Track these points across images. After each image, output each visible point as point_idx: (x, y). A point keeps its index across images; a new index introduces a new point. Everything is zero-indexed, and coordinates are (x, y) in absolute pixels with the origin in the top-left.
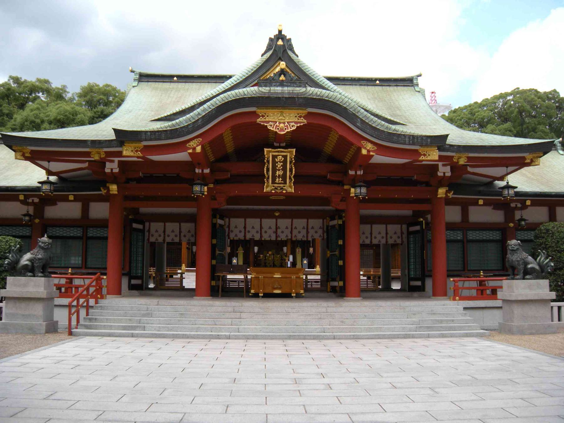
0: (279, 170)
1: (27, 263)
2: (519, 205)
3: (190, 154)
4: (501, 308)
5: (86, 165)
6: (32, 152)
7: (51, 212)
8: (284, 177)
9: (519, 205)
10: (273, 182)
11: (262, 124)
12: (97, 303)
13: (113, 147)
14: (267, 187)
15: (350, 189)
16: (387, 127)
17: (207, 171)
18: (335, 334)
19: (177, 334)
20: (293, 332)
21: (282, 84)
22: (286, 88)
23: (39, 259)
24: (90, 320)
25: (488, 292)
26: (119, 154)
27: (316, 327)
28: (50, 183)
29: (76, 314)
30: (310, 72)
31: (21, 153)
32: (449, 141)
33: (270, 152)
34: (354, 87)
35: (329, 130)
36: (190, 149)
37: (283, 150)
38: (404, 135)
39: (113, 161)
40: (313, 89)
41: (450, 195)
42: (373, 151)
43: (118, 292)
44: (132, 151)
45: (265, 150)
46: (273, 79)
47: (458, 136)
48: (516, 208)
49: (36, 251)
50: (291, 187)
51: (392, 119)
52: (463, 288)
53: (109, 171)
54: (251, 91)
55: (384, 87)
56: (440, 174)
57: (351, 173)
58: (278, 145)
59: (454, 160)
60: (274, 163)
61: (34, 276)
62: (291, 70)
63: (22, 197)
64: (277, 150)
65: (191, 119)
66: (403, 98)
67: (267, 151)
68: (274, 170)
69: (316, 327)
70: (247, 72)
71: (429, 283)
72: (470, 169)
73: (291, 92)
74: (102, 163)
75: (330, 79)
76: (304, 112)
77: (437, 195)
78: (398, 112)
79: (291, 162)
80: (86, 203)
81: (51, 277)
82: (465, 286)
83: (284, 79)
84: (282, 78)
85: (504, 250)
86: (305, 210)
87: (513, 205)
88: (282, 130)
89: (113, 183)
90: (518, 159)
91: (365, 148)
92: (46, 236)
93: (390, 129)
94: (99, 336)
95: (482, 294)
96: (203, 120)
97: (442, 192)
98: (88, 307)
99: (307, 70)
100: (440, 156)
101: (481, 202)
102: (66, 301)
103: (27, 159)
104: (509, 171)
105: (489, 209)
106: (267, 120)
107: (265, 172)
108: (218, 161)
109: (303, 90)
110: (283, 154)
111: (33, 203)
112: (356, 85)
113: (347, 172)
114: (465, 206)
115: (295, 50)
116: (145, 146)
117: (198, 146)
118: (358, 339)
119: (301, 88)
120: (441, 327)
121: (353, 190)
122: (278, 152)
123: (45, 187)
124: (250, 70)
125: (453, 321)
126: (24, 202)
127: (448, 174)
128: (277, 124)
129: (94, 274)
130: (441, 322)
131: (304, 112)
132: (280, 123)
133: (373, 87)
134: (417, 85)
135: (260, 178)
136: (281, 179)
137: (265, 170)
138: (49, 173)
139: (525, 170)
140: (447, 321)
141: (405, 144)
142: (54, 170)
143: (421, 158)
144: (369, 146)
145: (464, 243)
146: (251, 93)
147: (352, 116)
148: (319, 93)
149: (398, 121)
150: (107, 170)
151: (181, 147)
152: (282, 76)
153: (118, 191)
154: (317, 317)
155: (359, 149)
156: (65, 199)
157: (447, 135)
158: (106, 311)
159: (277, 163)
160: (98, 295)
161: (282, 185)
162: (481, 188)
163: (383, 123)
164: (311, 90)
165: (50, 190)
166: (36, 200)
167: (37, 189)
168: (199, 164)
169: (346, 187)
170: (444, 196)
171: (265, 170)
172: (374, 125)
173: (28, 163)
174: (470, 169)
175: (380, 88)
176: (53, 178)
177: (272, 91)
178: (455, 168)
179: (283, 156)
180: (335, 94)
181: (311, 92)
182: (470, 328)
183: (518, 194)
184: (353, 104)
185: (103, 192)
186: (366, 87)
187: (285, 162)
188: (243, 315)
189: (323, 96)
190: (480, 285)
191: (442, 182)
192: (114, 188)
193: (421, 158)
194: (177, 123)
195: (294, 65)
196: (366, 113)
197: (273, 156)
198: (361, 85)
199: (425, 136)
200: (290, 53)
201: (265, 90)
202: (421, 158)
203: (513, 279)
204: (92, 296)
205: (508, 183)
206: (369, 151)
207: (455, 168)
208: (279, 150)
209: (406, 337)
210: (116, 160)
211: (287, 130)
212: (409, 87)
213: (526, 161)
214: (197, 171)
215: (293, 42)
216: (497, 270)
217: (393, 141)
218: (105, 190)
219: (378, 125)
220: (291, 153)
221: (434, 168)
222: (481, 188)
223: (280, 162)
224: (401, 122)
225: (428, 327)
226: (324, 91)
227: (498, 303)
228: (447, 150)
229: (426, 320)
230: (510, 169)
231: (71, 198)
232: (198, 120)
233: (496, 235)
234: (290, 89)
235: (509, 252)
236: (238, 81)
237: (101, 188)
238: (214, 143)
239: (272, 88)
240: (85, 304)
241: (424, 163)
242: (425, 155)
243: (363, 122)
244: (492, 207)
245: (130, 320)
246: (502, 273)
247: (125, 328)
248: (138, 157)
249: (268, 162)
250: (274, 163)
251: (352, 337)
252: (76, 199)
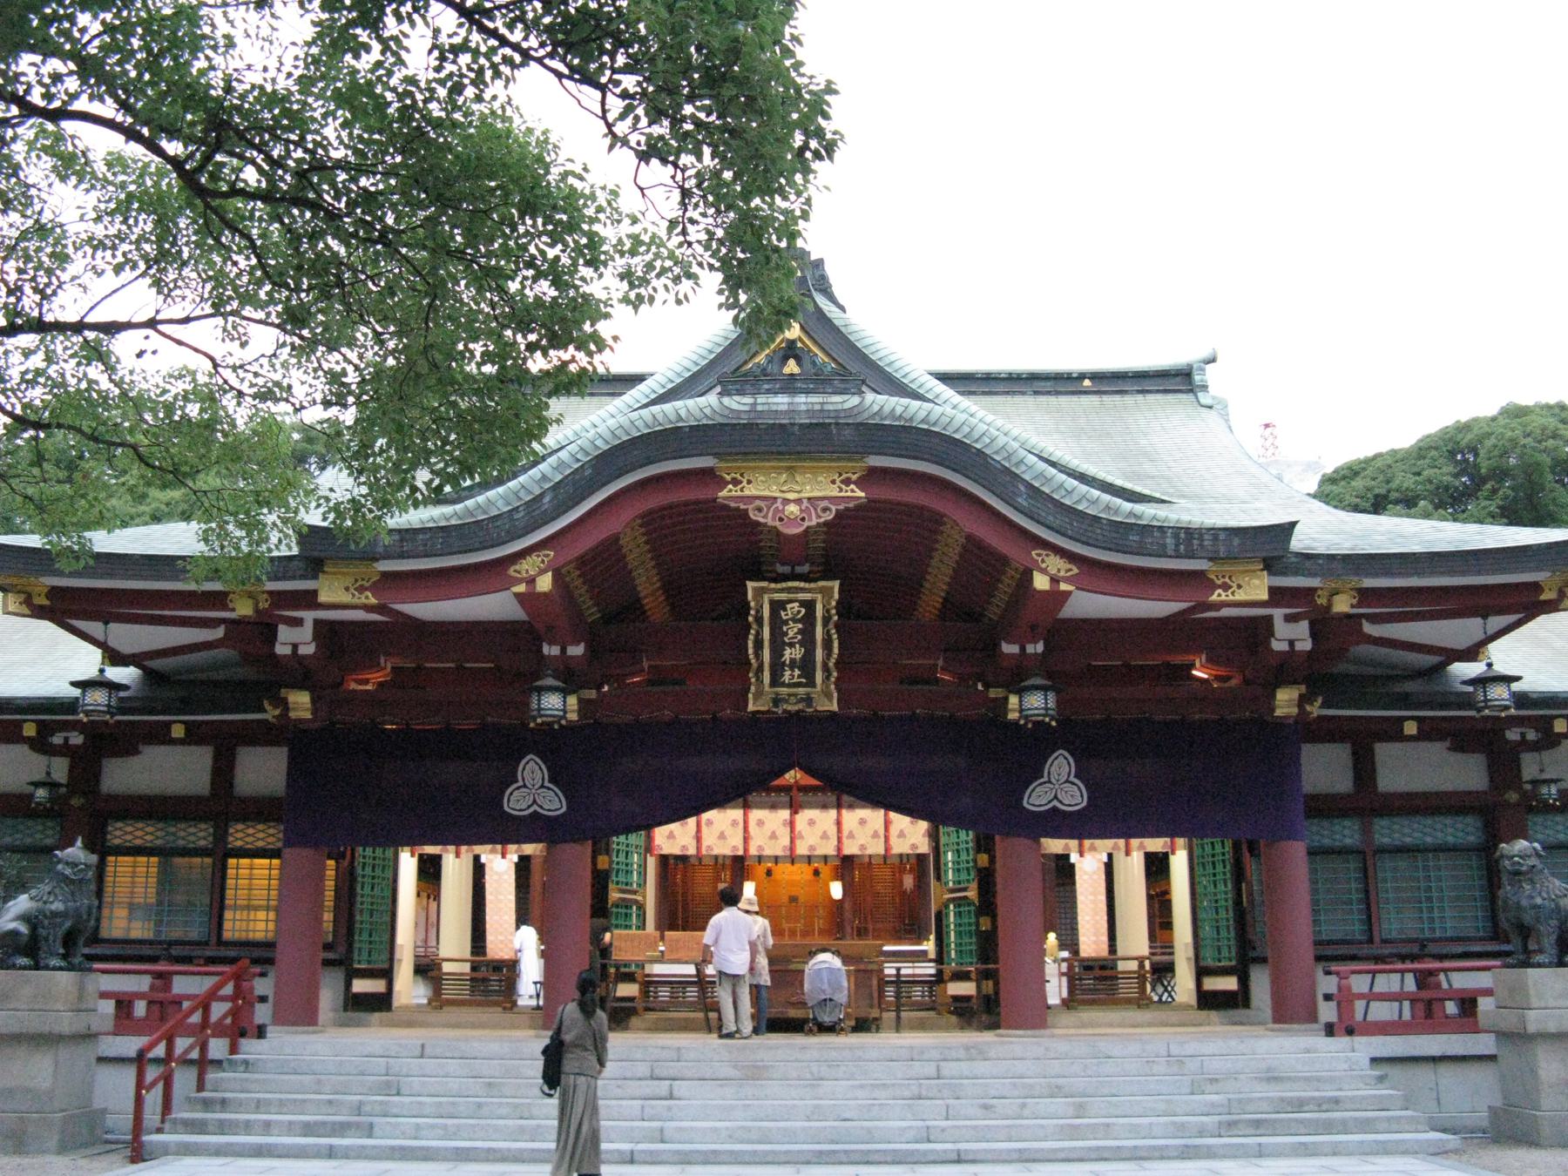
0: (791, 645)
1: (12, 926)
2: (1531, 735)
3: (517, 595)
4: (1492, 1058)
5: (219, 632)
6: (54, 592)
7: (126, 775)
8: (806, 665)
9: (1531, 735)
10: (775, 682)
11: (733, 505)
12: (234, 1049)
13: (293, 578)
14: (758, 695)
15: (1006, 699)
16: (1108, 508)
17: (576, 650)
18: (963, 1146)
20: (832, 1142)
21: (790, 385)
22: (801, 399)
23: (55, 914)
24: (207, 1104)
25: (1451, 1008)
26: (309, 600)
27: (904, 1124)
28: (112, 687)
29: (160, 1085)
30: (881, 354)
31: (23, 596)
32: (1298, 543)
33: (763, 590)
34: (1018, 399)
35: (938, 519)
36: (519, 581)
37: (802, 585)
38: (1160, 527)
39: (298, 622)
40: (881, 398)
41: (1315, 709)
42: (1068, 580)
43: (302, 1014)
44: (347, 589)
45: (750, 585)
46: (764, 372)
47: (1326, 530)
48: (1524, 744)
49: (48, 889)
50: (829, 696)
51: (1128, 486)
52: (1371, 997)
53: (287, 650)
55: (1105, 398)
56: (1278, 646)
57: (1009, 649)
58: (786, 569)
59: (1319, 601)
60: (777, 624)
61: (37, 967)
62: (823, 349)
63: (30, 730)
64: (784, 585)
65: (522, 494)
66: (1160, 424)
67: (754, 589)
68: (778, 646)
69: (904, 1124)
70: (695, 358)
71: (1261, 983)
72: (1368, 628)
73: (817, 407)
74: (264, 628)
75: (945, 378)
76: (856, 469)
77: (1273, 710)
78: (1148, 467)
79: (826, 620)
80: (225, 747)
81: (91, 970)
82: (1376, 989)
83: (796, 370)
84: (792, 367)
85: (1492, 873)
87: (1513, 735)
88: (793, 521)
89: (300, 686)
90: (1513, 596)
91: (1044, 571)
92: (79, 843)
93: (1116, 512)
94: (226, 1155)
95: (1429, 1014)
96: (555, 497)
97: (1286, 700)
98: (203, 1064)
99: (873, 349)
100: (1273, 591)
101: (1411, 728)
102: (130, 1045)
103: (39, 612)
104: (1490, 632)
105: (1436, 750)
106: (747, 493)
107: (751, 651)
108: (607, 619)
109: (854, 401)
110: (801, 596)
111: (66, 750)
112: (1023, 393)
113: (997, 646)
114: (1363, 743)
115: (837, 291)
117: (542, 572)
118: (1034, 1161)
119: (846, 397)
120: (1301, 1121)
121: (1013, 700)
122: (789, 590)
123: (98, 698)
124: (704, 353)
125: (1337, 1101)
126: (40, 744)
127: (1305, 645)
128: (779, 504)
129: (233, 961)
130: (1300, 1105)
131: (856, 469)
132: (786, 501)
133: (1075, 398)
134: (1204, 388)
136: (797, 672)
137: (750, 644)
138: (114, 657)
139: (1542, 625)
140: (1320, 1104)
141: (1162, 554)
142: (126, 648)
143: (1217, 596)
144: (1055, 564)
145: (1365, 858)
146: (698, 414)
147: (1002, 476)
148: (899, 410)
149: (1146, 492)
150: (282, 650)
151: (493, 574)
152: (792, 362)
153: (315, 711)
154: (907, 1093)
155: (1027, 576)
156: (159, 735)
157: (1293, 524)
158: (256, 1076)
159: (786, 622)
160: (241, 1029)
161: (801, 690)
162: (1410, 687)
163: (1096, 493)
164: (877, 403)
165: (108, 706)
166: (77, 739)
167: (70, 706)
168: (550, 628)
169: (994, 693)
170: (1295, 711)
171: (750, 644)
172: (1067, 502)
173: (47, 628)
174: (1368, 628)
175: (1094, 399)
176: (117, 674)
177: (759, 408)
178: (1323, 623)
179: (803, 603)
180: (948, 410)
181: (876, 408)
182: (1394, 1125)
183: (1522, 700)
184: (1002, 440)
185: (271, 713)
186: (1052, 399)
187: (809, 619)
188: (680, 1088)
189: (911, 419)
190: (1421, 984)
191: (1286, 669)
192: (300, 702)
193: (1214, 597)
194: (479, 506)
195: (826, 330)
196: (1042, 466)
197: (772, 602)
198: (1036, 393)
199: (1225, 529)
200: (821, 301)
201: (738, 403)
202: (1217, 596)
203: (1526, 964)
204: (220, 1031)
205: (1490, 665)
206: (1055, 580)
207: (1323, 623)
208: (790, 584)
209: (1187, 1153)
210: (309, 616)
211: (806, 524)
212: (1180, 396)
213: (1543, 597)
214: (546, 649)
215: (830, 270)
216: (1481, 939)
217: (1125, 546)
218: (276, 707)
219: (1079, 501)
220: (826, 594)
221: (1254, 631)
222: (1410, 687)
223: (795, 621)
224: (1157, 495)
225: (1257, 1124)
226: (916, 404)
227: (1483, 1044)
228: (1296, 572)
229: (1250, 1100)
230: (1496, 622)
231: (178, 731)
232: (542, 495)
233: (1465, 830)
234: (815, 399)
235: (1505, 879)
236: (670, 386)
237: (266, 704)
238: (597, 567)
239: (761, 399)
240: (195, 1055)
241: (1226, 612)
242: (1226, 587)
243: (1034, 492)
244: (1447, 744)
245: (330, 1102)
246: (1491, 947)
247: (308, 1129)
248: (368, 608)
249: (759, 620)
250: (777, 624)
251: (1015, 1156)
252: (195, 735)
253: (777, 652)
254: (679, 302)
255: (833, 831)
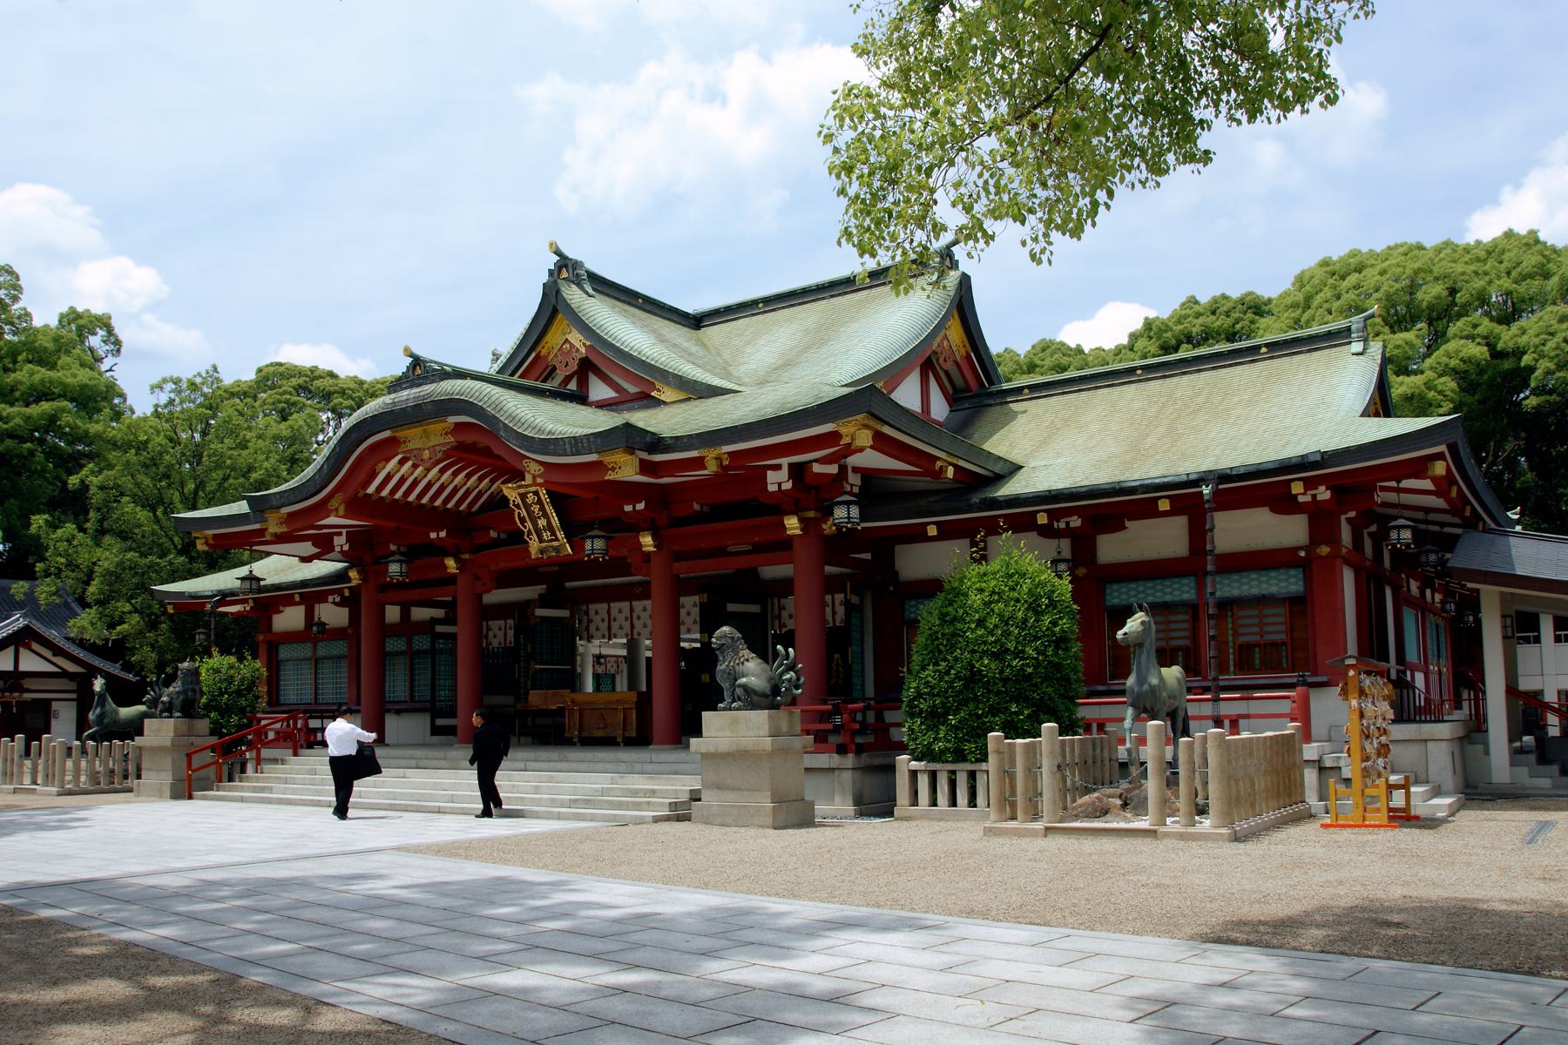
19: (505, 862)
39: (778, 467)
54: (407, 395)
63: (1042, 519)
86: (605, 586)
111: (1068, 532)
116: (290, 514)
135: (518, 538)
166: (1076, 522)
210: (785, 461)
231: (932, 531)
234: (415, 390)
253: (535, 524)
254: (1367, 15)
255: (635, 621)
